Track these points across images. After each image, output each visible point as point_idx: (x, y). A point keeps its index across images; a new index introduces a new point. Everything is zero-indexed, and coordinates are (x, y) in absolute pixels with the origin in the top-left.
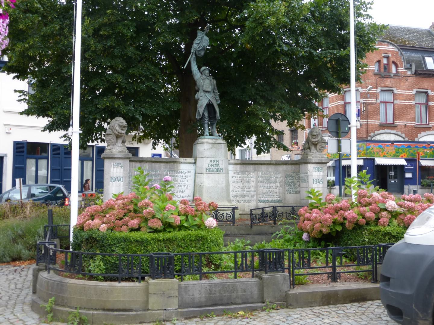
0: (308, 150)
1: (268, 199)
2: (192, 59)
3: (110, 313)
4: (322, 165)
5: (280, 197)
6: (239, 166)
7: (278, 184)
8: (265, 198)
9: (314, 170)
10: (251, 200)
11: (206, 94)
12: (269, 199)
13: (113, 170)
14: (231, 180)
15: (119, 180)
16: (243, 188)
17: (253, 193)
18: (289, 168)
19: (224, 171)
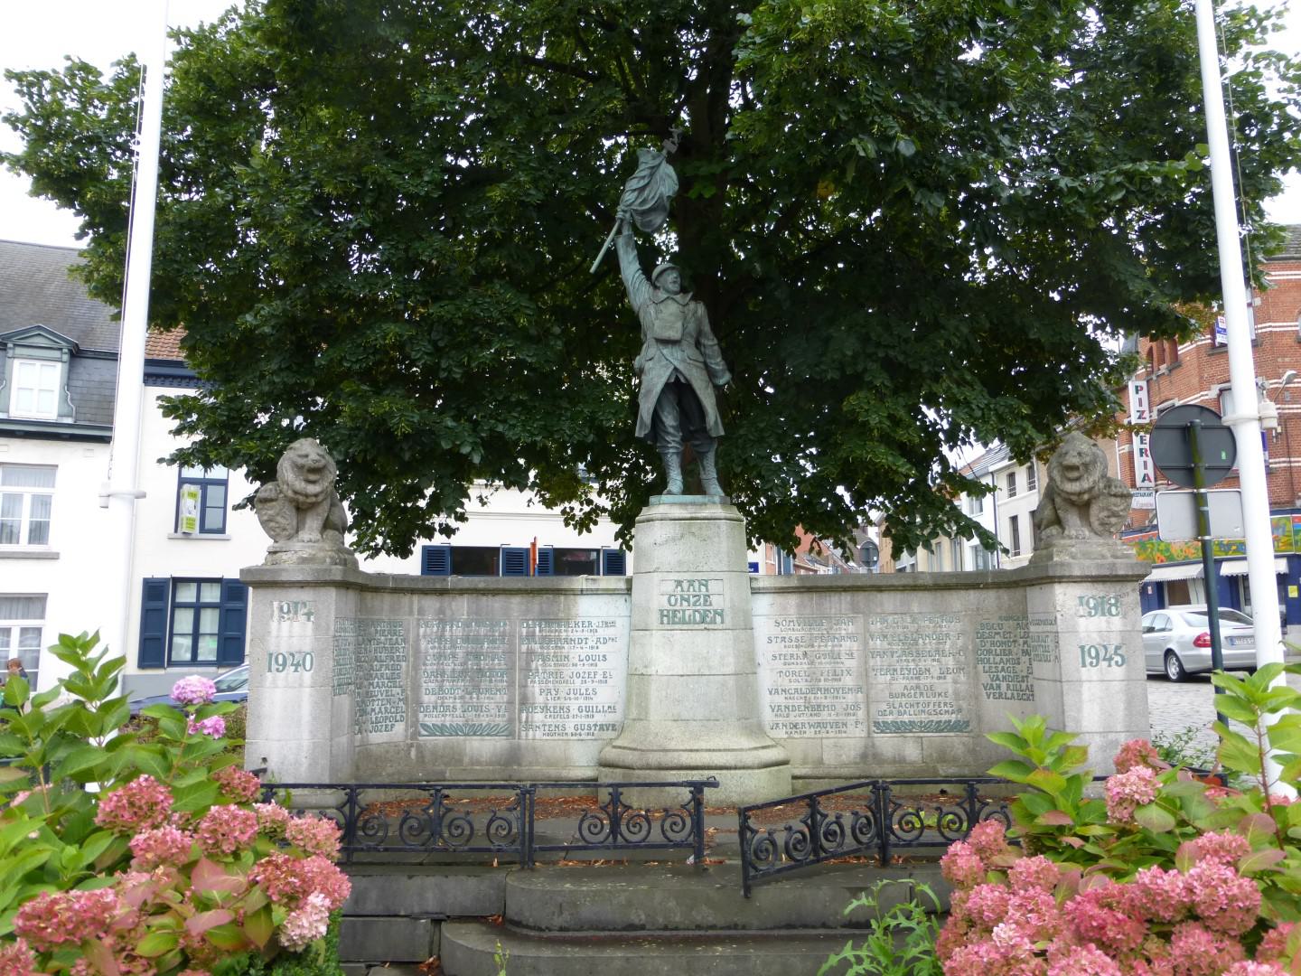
0: (1054, 530)
1: (913, 718)
2: (621, 241)
3: (617, 955)
4: (1118, 586)
5: (960, 710)
6: (793, 600)
7: (950, 662)
8: (900, 713)
9: (1082, 610)
10: (845, 725)
11: (665, 351)
12: (916, 719)
13: (279, 629)
14: (764, 651)
15: (297, 665)
16: (813, 677)
17: (850, 698)
18: (990, 598)
19: (728, 619)
